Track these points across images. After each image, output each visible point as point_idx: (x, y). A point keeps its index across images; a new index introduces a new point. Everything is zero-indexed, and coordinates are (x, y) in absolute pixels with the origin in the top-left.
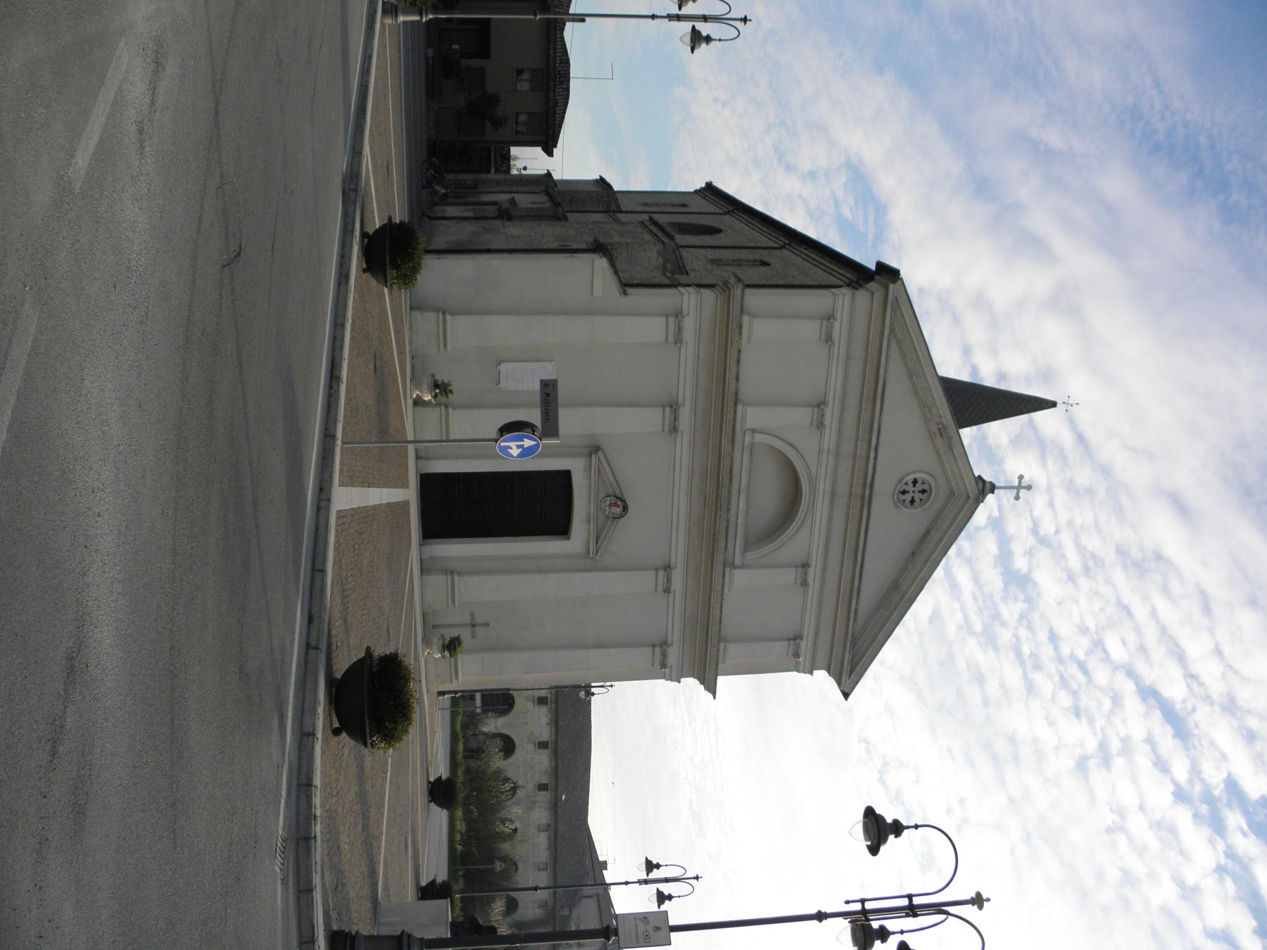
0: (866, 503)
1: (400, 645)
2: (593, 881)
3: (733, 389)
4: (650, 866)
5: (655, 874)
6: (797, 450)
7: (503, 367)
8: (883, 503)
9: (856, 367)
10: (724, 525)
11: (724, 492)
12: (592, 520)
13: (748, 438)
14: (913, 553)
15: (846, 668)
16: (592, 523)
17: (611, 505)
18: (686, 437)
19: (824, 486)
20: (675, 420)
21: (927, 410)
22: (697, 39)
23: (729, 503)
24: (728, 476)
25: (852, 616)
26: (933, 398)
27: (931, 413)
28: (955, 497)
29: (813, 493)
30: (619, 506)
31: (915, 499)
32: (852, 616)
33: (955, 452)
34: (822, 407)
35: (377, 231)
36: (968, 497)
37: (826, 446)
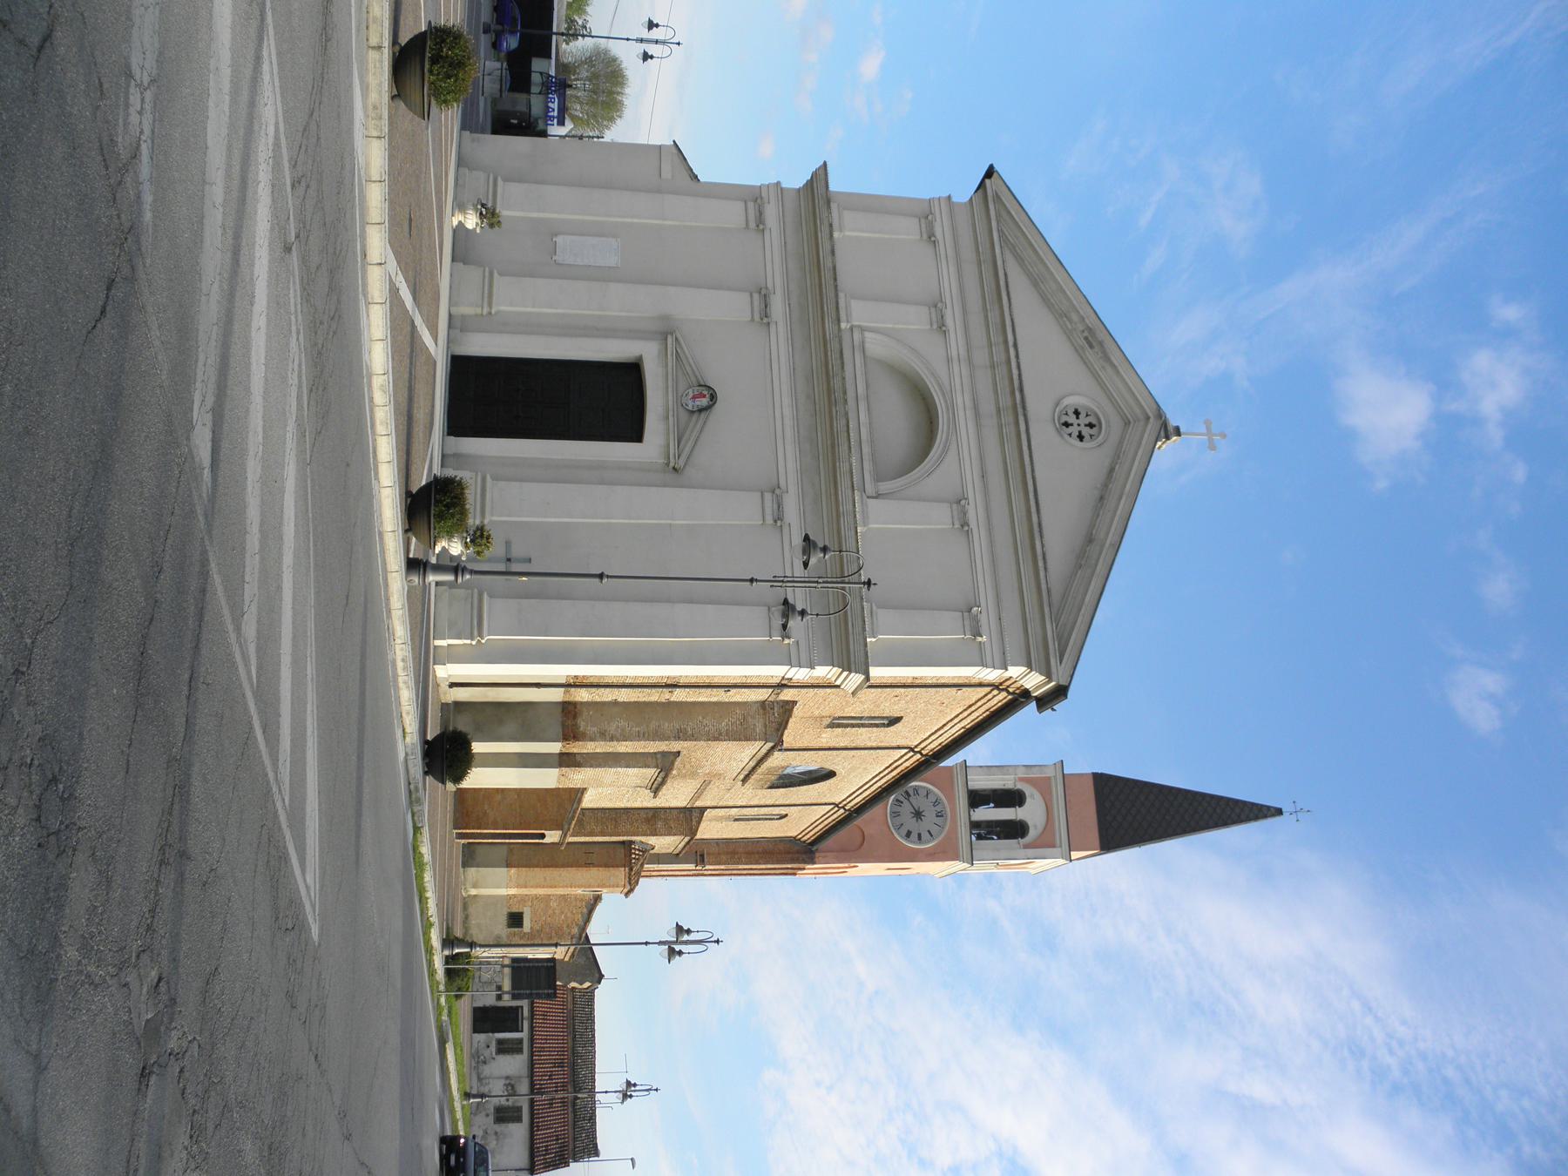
0: (1020, 410)
3: (829, 264)
7: (559, 240)
8: (1043, 434)
9: (970, 270)
10: (843, 422)
11: (837, 383)
12: (671, 413)
13: (857, 336)
14: (1102, 498)
15: (1053, 647)
16: (671, 418)
17: (694, 397)
18: (775, 233)
19: (962, 400)
20: (766, 307)
21: (1065, 319)
23: (845, 393)
24: (839, 362)
25: (1041, 564)
26: (1068, 299)
27: (1070, 320)
28: (1132, 425)
29: (951, 407)
30: (704, 396)
31: (1087, 423)
32: (1041, 564)
33: (1113, 358)
34: (963, 502)
35: (421, 489)
36: (1148, 418)
37: (954, 354)
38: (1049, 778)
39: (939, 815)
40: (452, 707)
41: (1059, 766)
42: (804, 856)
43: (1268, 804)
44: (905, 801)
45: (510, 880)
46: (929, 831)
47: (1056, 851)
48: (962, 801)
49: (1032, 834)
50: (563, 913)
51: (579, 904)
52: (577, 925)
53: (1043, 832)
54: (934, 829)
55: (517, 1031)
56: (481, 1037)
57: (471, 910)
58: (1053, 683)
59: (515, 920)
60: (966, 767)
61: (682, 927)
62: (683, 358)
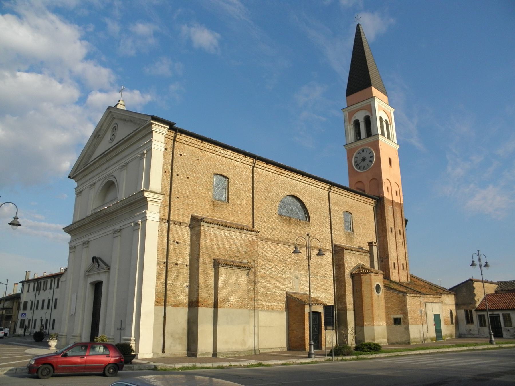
1: (451, 344)
2: (485, 286)
4: (473, 264)
5: (477, 262)
6: (116, 179)
18: (90, 237)
22: (486, 265)
27: (95, 144)
38: (349, 113)
39: (363, 151)
40: (189, 352)
41: (344, 110)
42: (382, 201)
43: (356, 30)
44: (360, 165)
45: (370, 325)
46: (369, 154)
47: (372, 103)
48: (359, 143)
49: (368, 114)
50: (393, 301)
51: (389, 294)
52: (398, 294)
53: (365, 109)
54: (368, 152)
55: (499, 317)
56: (505, 334)
57: (394, 341)
58: (152, 121)
59: (397, 321)
60: (346, 145)
61: (294, 251)
62: (90, 269)
